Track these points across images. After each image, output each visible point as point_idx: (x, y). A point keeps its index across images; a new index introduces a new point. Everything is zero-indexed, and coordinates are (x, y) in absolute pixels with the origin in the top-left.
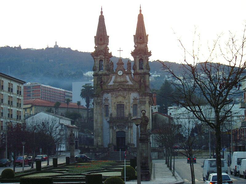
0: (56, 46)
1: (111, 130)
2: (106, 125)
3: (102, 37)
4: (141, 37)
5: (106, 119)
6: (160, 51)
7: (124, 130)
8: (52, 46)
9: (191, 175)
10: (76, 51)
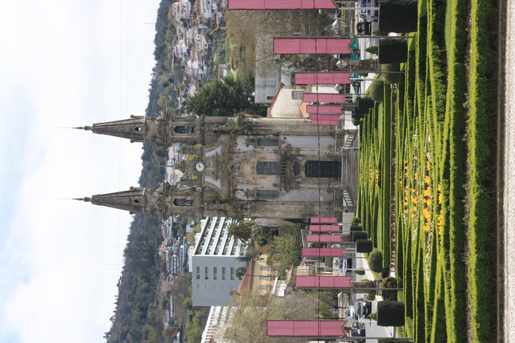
0: (149, 96)
1: (301, 185)
2: (293, 195)
5: (283, 195)
7: (303, 163)
8: (149, 93)
10: (160, 4)
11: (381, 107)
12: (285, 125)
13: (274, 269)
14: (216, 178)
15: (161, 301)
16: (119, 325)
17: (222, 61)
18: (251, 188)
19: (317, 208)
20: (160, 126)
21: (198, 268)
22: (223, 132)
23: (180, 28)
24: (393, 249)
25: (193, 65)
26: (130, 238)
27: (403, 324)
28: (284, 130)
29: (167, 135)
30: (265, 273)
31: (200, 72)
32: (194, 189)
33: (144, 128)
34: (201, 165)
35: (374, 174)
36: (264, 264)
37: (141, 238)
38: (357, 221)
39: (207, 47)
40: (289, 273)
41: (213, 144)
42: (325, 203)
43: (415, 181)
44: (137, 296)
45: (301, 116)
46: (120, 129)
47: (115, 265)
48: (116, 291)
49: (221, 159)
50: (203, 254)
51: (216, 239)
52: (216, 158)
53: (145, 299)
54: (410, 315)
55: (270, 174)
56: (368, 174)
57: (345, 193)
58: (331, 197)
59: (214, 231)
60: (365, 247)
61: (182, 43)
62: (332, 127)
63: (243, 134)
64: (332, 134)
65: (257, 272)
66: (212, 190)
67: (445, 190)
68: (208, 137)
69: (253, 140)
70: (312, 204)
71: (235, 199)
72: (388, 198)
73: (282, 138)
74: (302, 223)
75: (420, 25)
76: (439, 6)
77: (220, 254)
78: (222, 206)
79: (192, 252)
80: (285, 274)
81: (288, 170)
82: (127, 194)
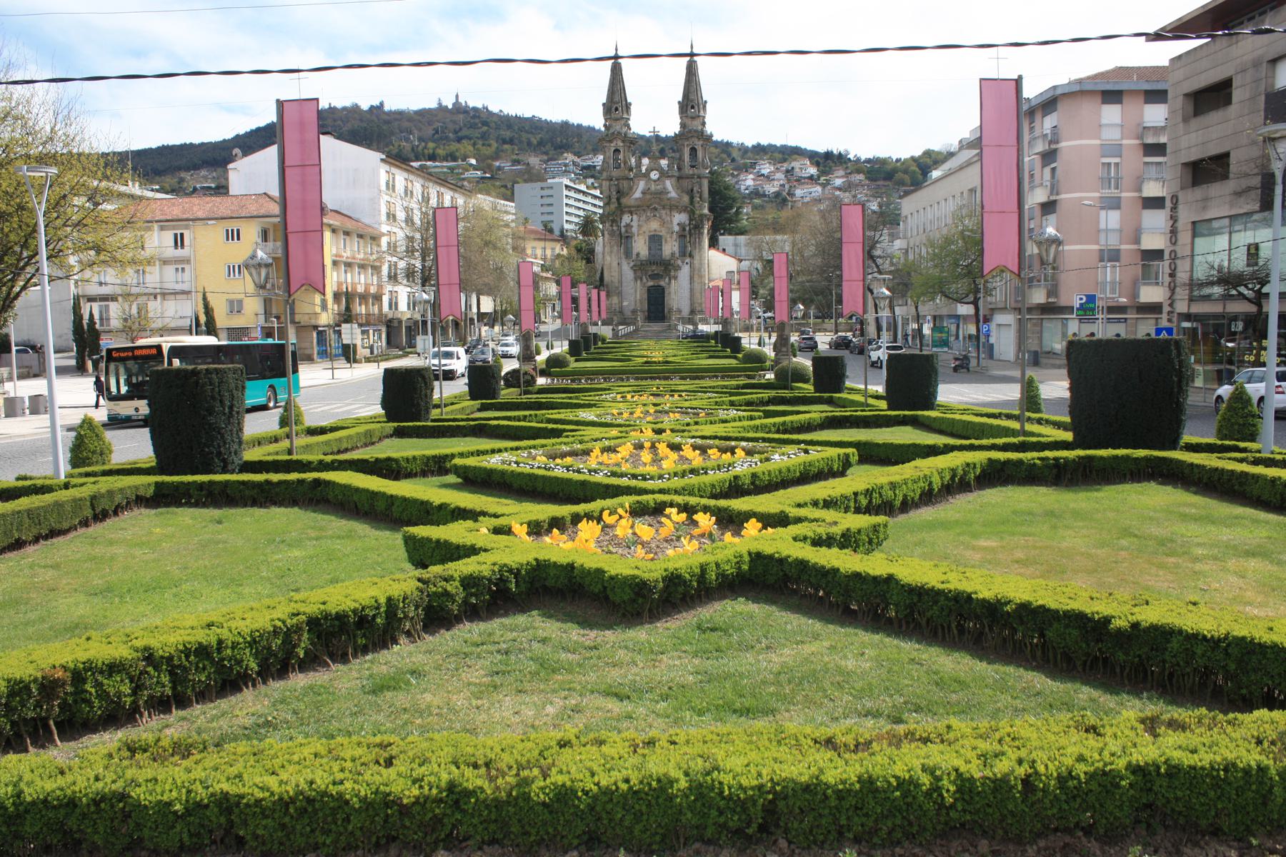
3: (616, 103)
4: (691, 103)
6: (722, 125)
7: (662, 283)
9: (361, 528)
11: (733, 362)
12: (701, 264)
13: (553, 261)
14: (643, 193)
15: (520, 157)
16: (495, 119)
17: (755, 208)
18: (634, 230)
19: (615, 300)
20: (696, 131)
22: (692, 198)
23: (785, 166)
24: (573, 381)
25: (749, 181)
26: (579, 126)
27: (473, 398)
28: (696, 262)
29: (687, 139)
30: (549, 253)
31: (743, 187)
32: (631, 170)
35: (657, 356)
36: (558, 250)
37: (580, 136)
38: (603, 340)
40: (549, 275)
41: (679, 188)
42: (621, 307)
43: (667, 412)
44: (524, 135)
45: (710, 281)
46: (692, 89)
47: (553, 114)
48: (528, 115)
49: (664, 197)
50: (566, 192)
51: (581, 205)
52: (664, 192)
53: (521, 142)
54: (483, 408)
55: (650, 249)
56: (656, 351)
57: (632, 328)
58: (628, 313)
59: (587, 203)
60: (575, 349)
62: (701, 312)
63: (691, 220)
64: (692, 312)
65: (549, 245)
66: (631, 188)
67: (717, 565)
68: (685, 183)
69: (684, 230)
70: (620, 294)
71: (622, 213)
72: (632, 372)
73: (688, 260)
74: (600, 284)
75: (905, 416)
76: (1055, 471)
77: (566, 209)
78: (614, 200)
79: (566, 182)
80: (547, 271)
81: (654, 267)
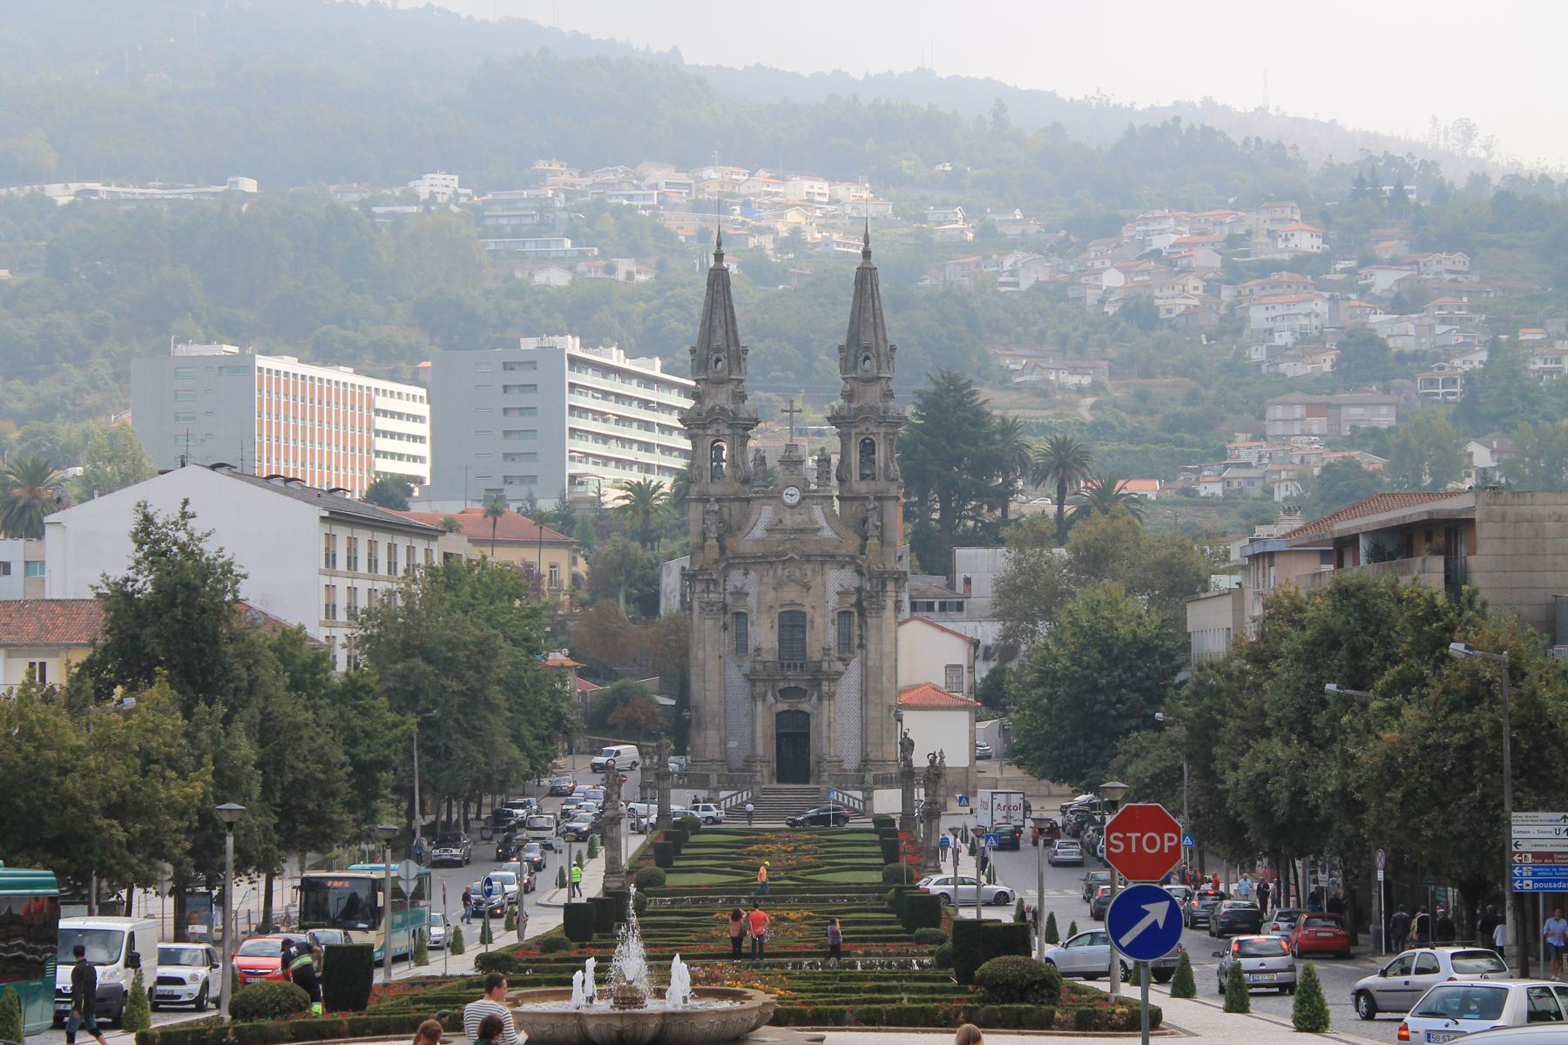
7: (805, 707)
21: (532, 365)
31: (1092, 297)
33: (870, 375)
34: (795, 499)
39: (1163, 315)
59: (628, 399)
61: (1181, 233)
64: (865, 762)
66: (746, 516)
78: (712, 542)
82: (732, 341)
